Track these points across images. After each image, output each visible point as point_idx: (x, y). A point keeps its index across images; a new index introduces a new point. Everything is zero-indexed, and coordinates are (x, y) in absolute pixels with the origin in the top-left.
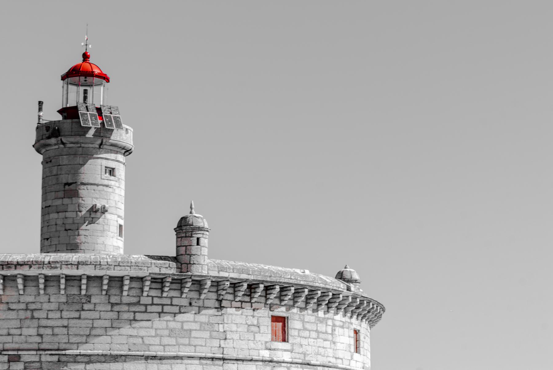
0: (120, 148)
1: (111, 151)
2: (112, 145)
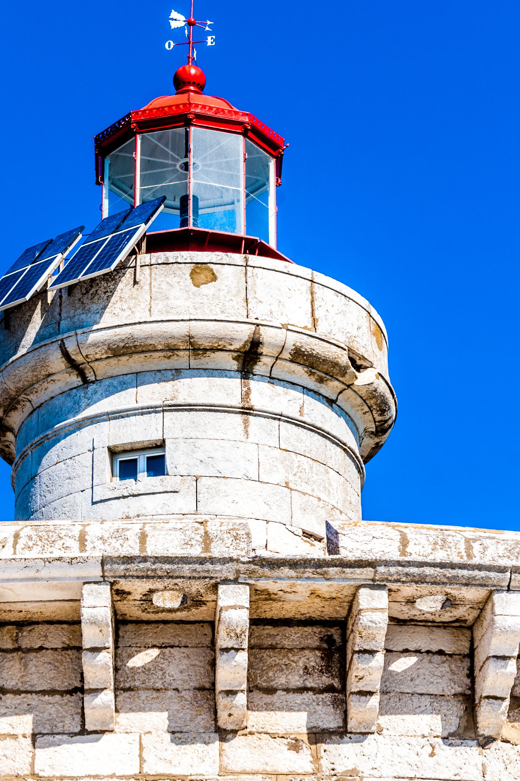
0: (171, 349)
1: (138, 378)
2: (117, 351)
